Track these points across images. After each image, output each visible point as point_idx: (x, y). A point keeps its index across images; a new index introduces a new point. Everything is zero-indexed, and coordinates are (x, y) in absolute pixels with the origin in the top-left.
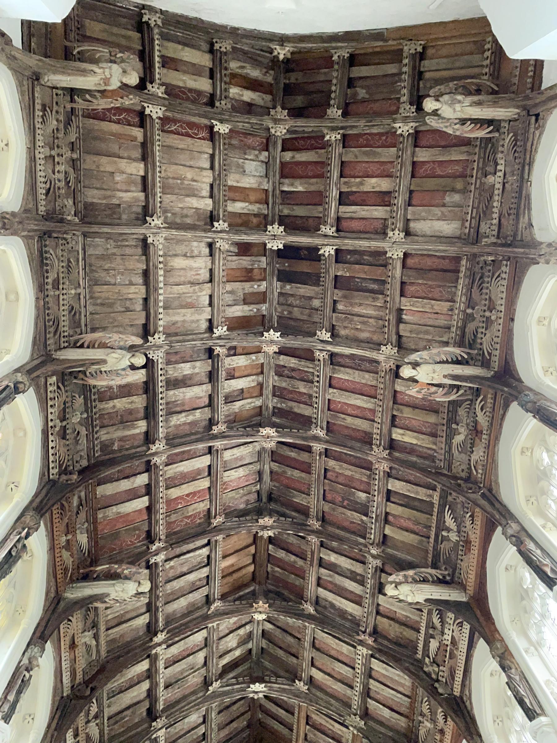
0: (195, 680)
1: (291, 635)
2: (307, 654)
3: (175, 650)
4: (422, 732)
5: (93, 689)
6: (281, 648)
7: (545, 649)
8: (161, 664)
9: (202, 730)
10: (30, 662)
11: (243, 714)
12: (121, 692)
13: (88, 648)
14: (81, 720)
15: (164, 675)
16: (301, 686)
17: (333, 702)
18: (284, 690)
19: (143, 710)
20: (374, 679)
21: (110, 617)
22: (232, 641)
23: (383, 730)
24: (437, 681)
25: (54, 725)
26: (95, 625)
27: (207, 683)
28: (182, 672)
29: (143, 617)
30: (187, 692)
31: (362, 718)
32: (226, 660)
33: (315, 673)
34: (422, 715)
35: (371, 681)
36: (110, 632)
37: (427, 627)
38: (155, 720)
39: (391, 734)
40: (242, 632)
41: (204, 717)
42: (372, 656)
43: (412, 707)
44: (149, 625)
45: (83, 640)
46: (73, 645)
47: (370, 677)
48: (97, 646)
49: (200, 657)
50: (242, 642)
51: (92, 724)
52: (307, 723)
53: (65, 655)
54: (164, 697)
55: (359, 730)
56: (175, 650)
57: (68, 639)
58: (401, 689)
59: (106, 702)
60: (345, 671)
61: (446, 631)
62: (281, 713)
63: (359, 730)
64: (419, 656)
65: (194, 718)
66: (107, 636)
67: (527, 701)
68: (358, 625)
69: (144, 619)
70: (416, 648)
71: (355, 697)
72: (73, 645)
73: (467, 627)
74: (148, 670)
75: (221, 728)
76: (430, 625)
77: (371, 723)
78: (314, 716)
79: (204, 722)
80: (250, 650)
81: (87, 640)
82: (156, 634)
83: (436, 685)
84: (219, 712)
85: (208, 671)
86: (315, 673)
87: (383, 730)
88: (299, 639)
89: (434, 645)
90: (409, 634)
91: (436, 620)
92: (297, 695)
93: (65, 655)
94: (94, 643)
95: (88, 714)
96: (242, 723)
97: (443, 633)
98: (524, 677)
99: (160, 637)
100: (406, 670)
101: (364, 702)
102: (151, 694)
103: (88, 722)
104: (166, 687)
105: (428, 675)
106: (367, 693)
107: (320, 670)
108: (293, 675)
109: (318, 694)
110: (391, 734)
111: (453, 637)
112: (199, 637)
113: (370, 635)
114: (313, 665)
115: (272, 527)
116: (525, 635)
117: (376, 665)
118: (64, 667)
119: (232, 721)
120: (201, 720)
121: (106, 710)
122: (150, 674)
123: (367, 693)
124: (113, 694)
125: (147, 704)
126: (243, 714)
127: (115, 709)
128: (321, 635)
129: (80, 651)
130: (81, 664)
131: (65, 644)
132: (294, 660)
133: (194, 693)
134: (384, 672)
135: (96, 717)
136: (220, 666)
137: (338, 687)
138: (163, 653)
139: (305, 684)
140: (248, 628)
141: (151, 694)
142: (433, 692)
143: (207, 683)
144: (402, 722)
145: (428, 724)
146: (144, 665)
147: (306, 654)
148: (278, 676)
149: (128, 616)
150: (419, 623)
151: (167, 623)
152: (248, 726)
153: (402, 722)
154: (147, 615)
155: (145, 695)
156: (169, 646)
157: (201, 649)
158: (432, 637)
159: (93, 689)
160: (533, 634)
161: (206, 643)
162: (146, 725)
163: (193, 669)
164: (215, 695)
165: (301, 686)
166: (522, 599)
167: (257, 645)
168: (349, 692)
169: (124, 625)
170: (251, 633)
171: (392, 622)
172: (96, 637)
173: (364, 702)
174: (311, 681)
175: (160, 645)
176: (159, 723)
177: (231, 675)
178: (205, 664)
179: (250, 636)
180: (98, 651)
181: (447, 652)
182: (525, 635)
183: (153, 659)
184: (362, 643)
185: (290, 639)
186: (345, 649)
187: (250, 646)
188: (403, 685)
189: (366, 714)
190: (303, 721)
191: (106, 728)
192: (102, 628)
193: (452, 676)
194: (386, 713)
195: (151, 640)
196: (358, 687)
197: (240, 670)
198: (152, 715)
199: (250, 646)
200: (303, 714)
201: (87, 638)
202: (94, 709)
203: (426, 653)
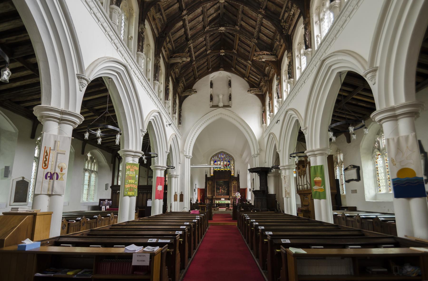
0: (200, 26)
1: (234, 7)
2: (240, 16)
3: (191, 16)
4: (275, 45)
5: (166, 34)
6: (230, 13)
7: (323, 22)
8: (187, 22)
9: (204, 43)
10: (142, 30)
11: (218, 36)
12: (175, 33)
13: (160, 19)
14: (165, 44)
15: (188, 26)
16: (237, 28)
17: (248, 33)
18: (231, 30)
19: (184, 38)
20: (263, 26)
21: (164, 6)
22: (212, 11)
23: (263, 43)
24: (284, 29)
25: (157, 47)
26: (160, 10)
27: (204, 27)
28: (195, 24)
29: (176, 5)
30: (198, 31)
31: (257, 40)
32: (210, 19)
33: (237, 66)
34: (277, 40)
35: (262, 27)
36: (166, 12)
37: (286, 8)
38: (188, 41)
39: (265, 45)
40: (216, 6)
41: (205, 38)
42: (263, 18)
43: (274, 36)
44: (179, 7)
45: (157, 17)
46: (154, 19)
47: (262, 25)
48: (163, 17)
49: (201, 18)
50: (216, 11)
51: (169, 44)
52: (239, 40)
53: (153, 23)
54: (190, 33)
55: (255, 43)
56: (191, 16)
57: (151, 17)
58: (272, 30)
59: (171, 37)
60: (253, 23)
61: (292, 10)
62: (231, 36)
63: (255, 43)
64: (280, 18)
65: (201, 39)
66: (165, 13)
67: (307, 43)
68: (260, 5)
69: (177, 6)
70: (280, 15)
71: (256, 34)
72: (154, 19)
73: (299, 11)
74: (183, 25)
75: (211, 41)
76: (287, 7)
77: (260, 41)
78: (241, 38)
79: (205, 40)
80: (219, 14)
81: (158, 16)
82: (183, 11)
83: (283, 30)
84: (210, 37)
85: (204, 23)
86: (243, 24)
87: (263, 43)
88: (237, 10)
89: (286, 15)
90: (278, 9)
91: (290, 5)
92: (236, 31)
93: (153, 23)
94: (161, 17)
95: (166, 41)
96: (218, 39)
97: (291, 11)
98: (310, 34)
99: (185, 12)
100: (274, 24)
101: (258, 34)
102: (186, 32)
103: (167, 44)
104: (190, 30)
105: (282, 26)
106: (260, 31)
107: (245, 22)
108: (235, 24)
109: (243, 30)
110: (265, 45)
111: (294, 12)
112: (199, 10)
113: (264, 10)
114: (242, 20)
115: (223, 53)
116: (319, 15)
117: (265, 21)
118: (154, 28)
119: (214, 39)
120: (204, 39)
121: (172, 39)
122: (184, 26)
123: (260, 31)
124: (173, 34)
125: (185, 36)
126: (218, 36)
127: (175, 38)
128: (246, 8)
129: (157, 21)
130: (159, 25)
131: (151, 19)
132: (235, 17)
133: (200, 31)
134: (267, 24)
135: (169, 42)
136: (208, 20)
137: (250, 29)
138: (187, 18)
139: (239, 27)
140: (218, 4)
141: (186, 32)
142: (281, 33)
143: (204, 27)
144: (269, 41)
145: (278, 43)
146: (181, 23)
147: (240, 16)
148: (230, 24)
149: (171, 4)
150: (283, 5)
151: (186, 6)
152: (220, 40)
153: (269, 41)
154: (178, 3)
155: (183, 33)
156: (188, 15)
157: (200, 15)
158: (287, 12)
159: (166, 34)
160: (321, 16)
161: (202, 12)
162: (186, 43)
163: (199, 22)
164: (208, 32)
165: (237, 28)
166: (228, 185)
167: (222, 11)
168: (254, 30)
169: (170, 9)
170: (219, 6)
171: (273, 4)
172: (161, 14)
173: (258, 34)
174: (241, 26)
175: (185, 15)
176: (190, 42)
177: (213, 24)
178: (203, 20)
179: (219, 8)
180: (164, 20)
181: (291, 18)
182: (319, 15)
183: (184, 21)
184: (260, 13)
185: (234, 9)
186: (254, 14)
187: (219, 12)
188: (272, 29)
189: (258, 38)
190: (238, 40)
191: (173, 45)
192: (163, 11)
193: (289, 28)
194: (265, 38)
195: (181, 14)
196: (257, 29)
197: (216, 21)
198: (187, 40)
199: (219, 12)
200: (238, 37)
201: (158, 16)
202: (168, 40)
203: (283, 18)
